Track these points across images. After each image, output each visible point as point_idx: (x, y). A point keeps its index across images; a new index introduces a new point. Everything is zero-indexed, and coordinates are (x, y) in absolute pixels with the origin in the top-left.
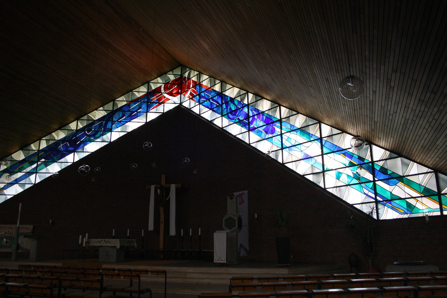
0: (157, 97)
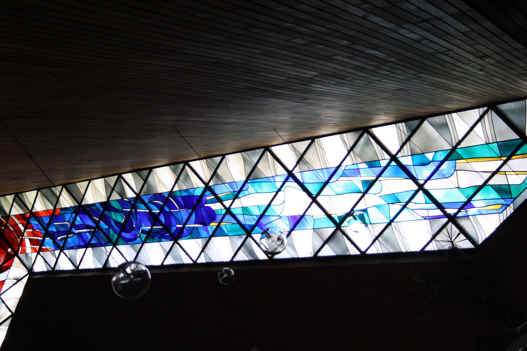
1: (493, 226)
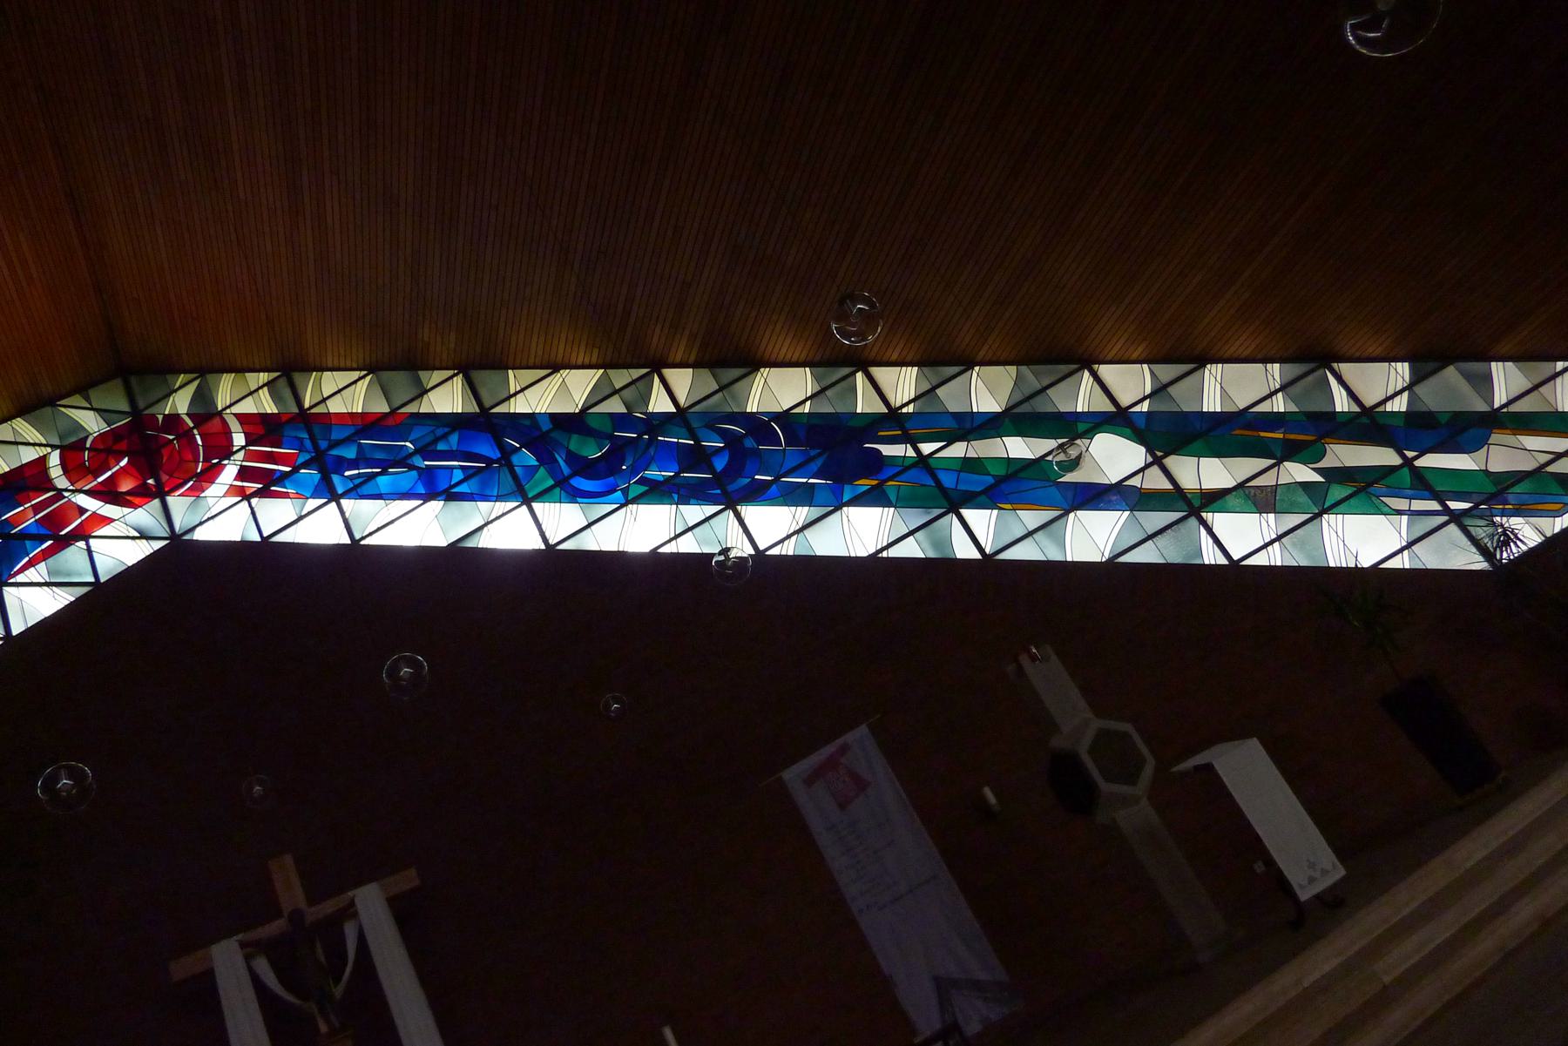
0: (37, 509)
1: (339, 391)
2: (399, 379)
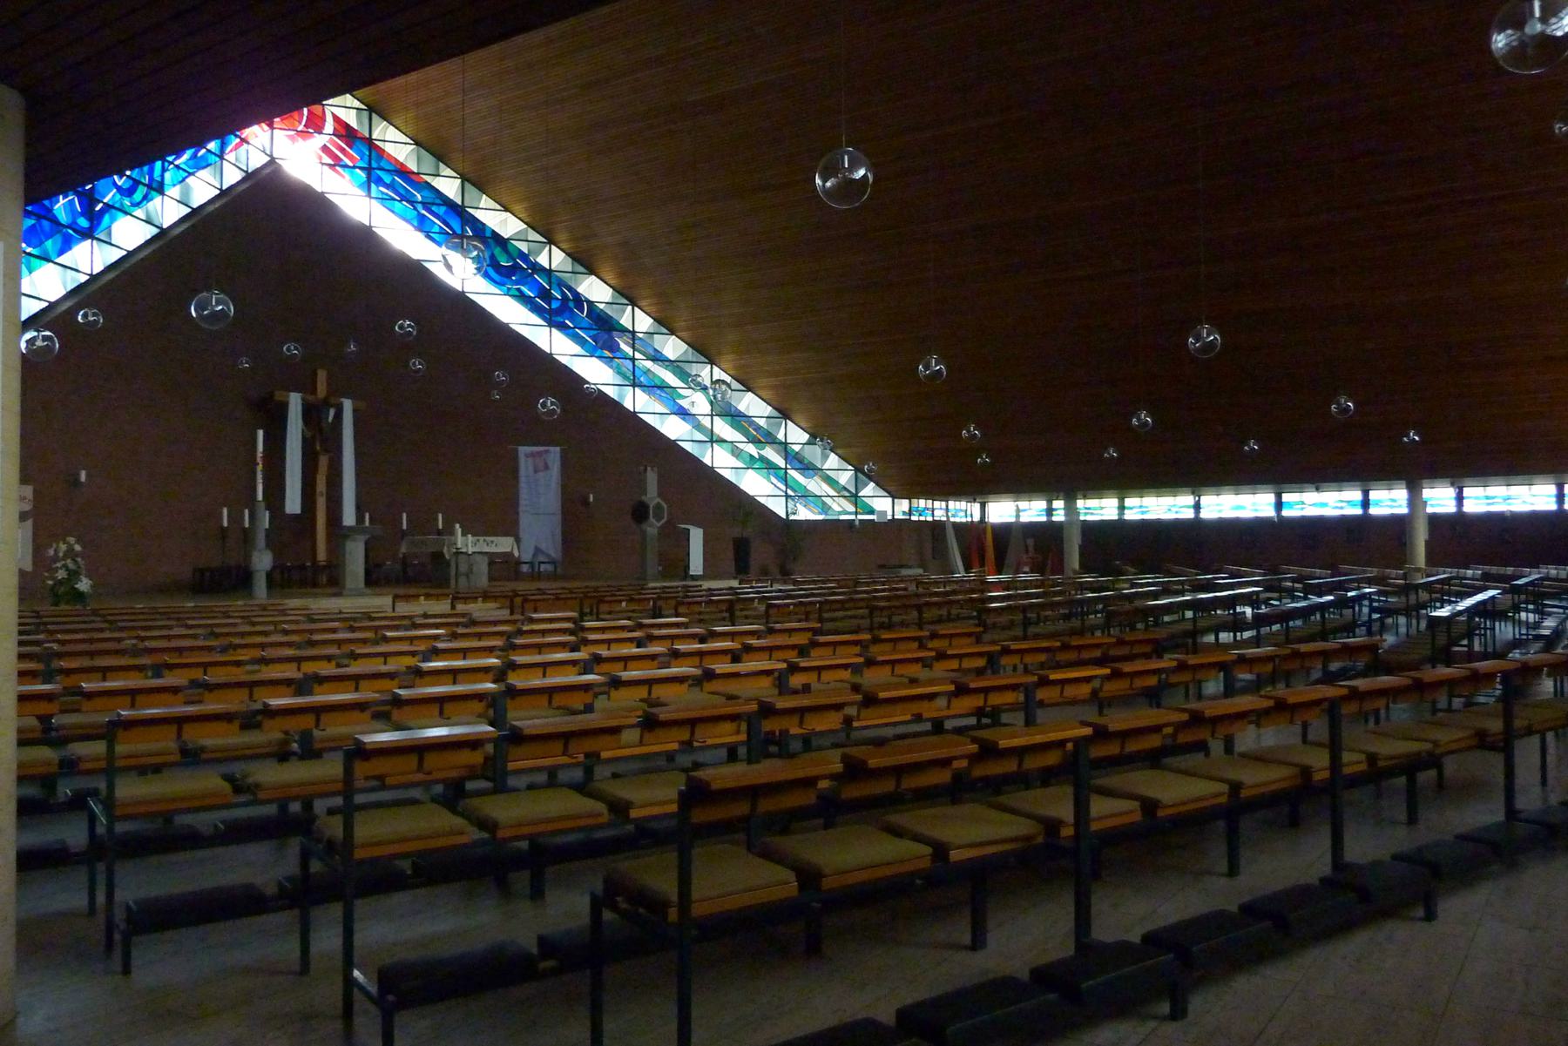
2: (429, 159)
